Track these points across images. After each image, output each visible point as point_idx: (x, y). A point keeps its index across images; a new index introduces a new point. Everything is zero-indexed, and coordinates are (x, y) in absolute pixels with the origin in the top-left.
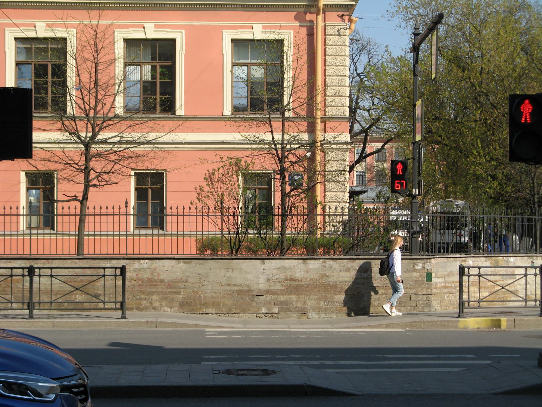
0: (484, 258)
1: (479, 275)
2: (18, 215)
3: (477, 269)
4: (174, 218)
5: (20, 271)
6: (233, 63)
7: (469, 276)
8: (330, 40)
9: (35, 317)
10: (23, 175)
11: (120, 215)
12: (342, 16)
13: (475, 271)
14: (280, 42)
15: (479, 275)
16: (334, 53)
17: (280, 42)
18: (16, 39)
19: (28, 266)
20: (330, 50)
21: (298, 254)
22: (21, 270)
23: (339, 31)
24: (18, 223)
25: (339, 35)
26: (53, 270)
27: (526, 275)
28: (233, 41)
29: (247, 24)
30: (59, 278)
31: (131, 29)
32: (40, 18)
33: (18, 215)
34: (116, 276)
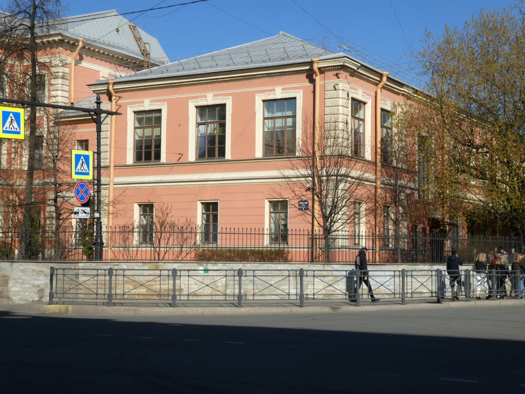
0: (141, 264)
1: (64, 275)
2: (263, 234)
3: (252, 272)
4: (224, 235)
5: (232, 273)
6: (197, 123)
7: (116, 275)
8: (328, 94)
9: (242, 305)
10: (267, 204)
11: (243, 234)
12: (337, 75)
13: (251, 273)
14: (223, 106)
15: (254, 276)
16: (330, 105)
17: (223, 106)
18: (135, 112)
19: (172, 268)
20: (328, 102)
21: (73, 260)
22: (122, 271)
23: (334, 87)
24: (263, 239)
25: (335, 89)
26: (190, 272)
27: (289, 276)
28: (264, 101)
29: (271, 88)
30: (196, 278)
31: (199, 99)
32: (277, 84)
33: (263, 234)
34: (169, 276)
